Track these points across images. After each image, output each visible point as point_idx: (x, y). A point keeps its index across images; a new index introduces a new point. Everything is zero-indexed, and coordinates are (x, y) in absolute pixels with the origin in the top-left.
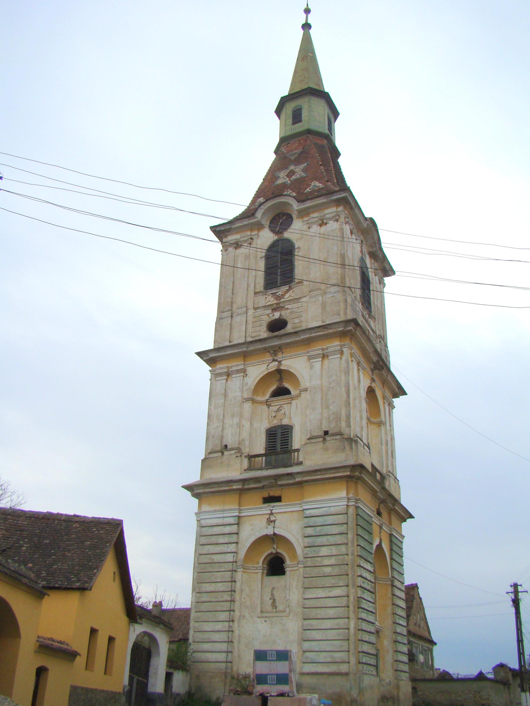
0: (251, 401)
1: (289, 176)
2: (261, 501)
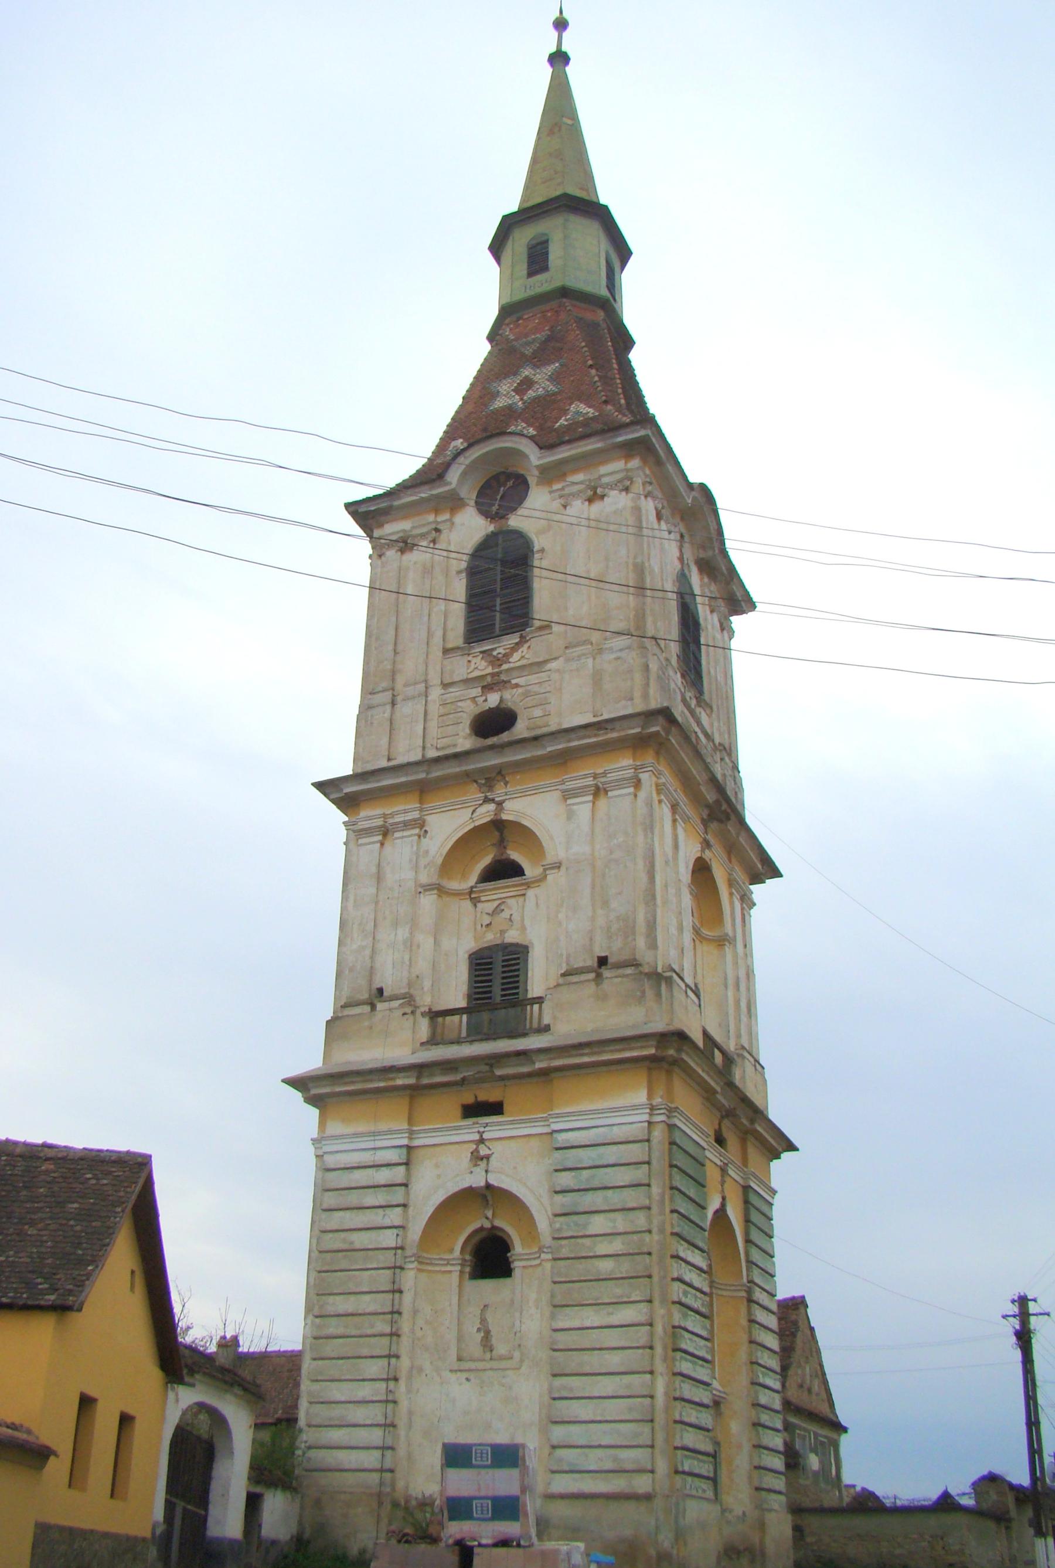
0: (435, 892)
1: (520, 390)
2: (458, 1112)
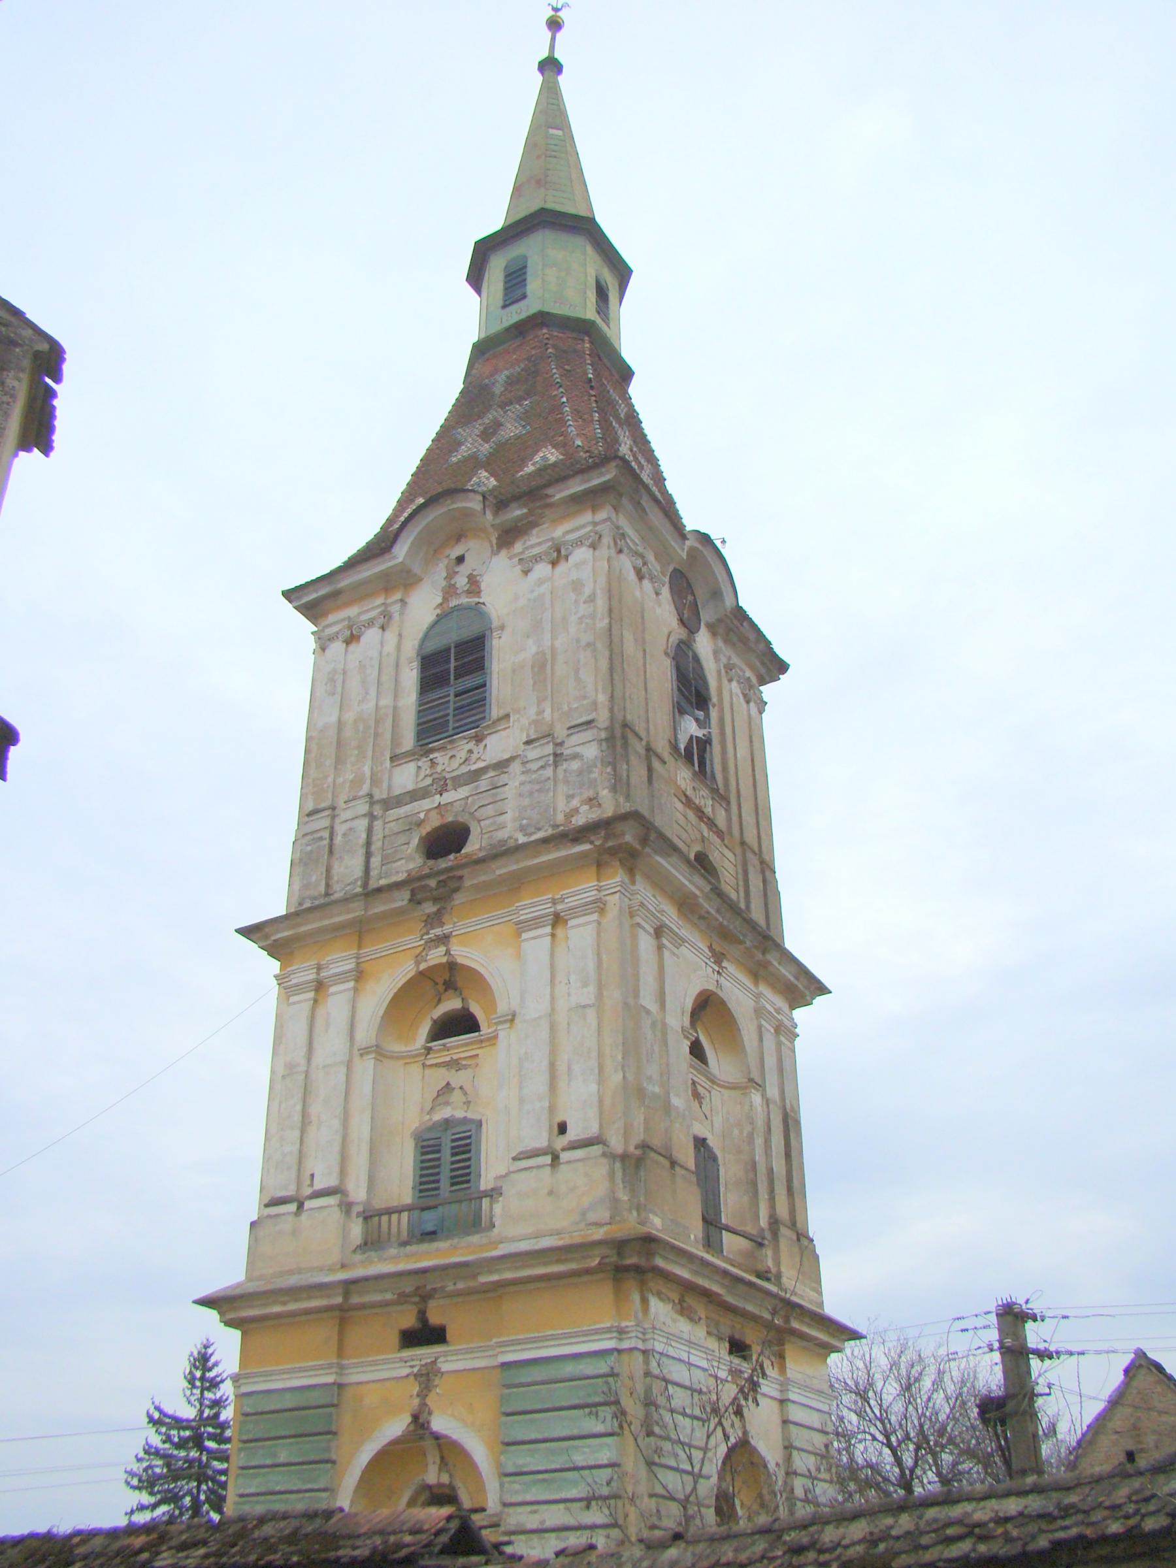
0: (373, 1055)
1: (486, 435)
2: (395, 1339)
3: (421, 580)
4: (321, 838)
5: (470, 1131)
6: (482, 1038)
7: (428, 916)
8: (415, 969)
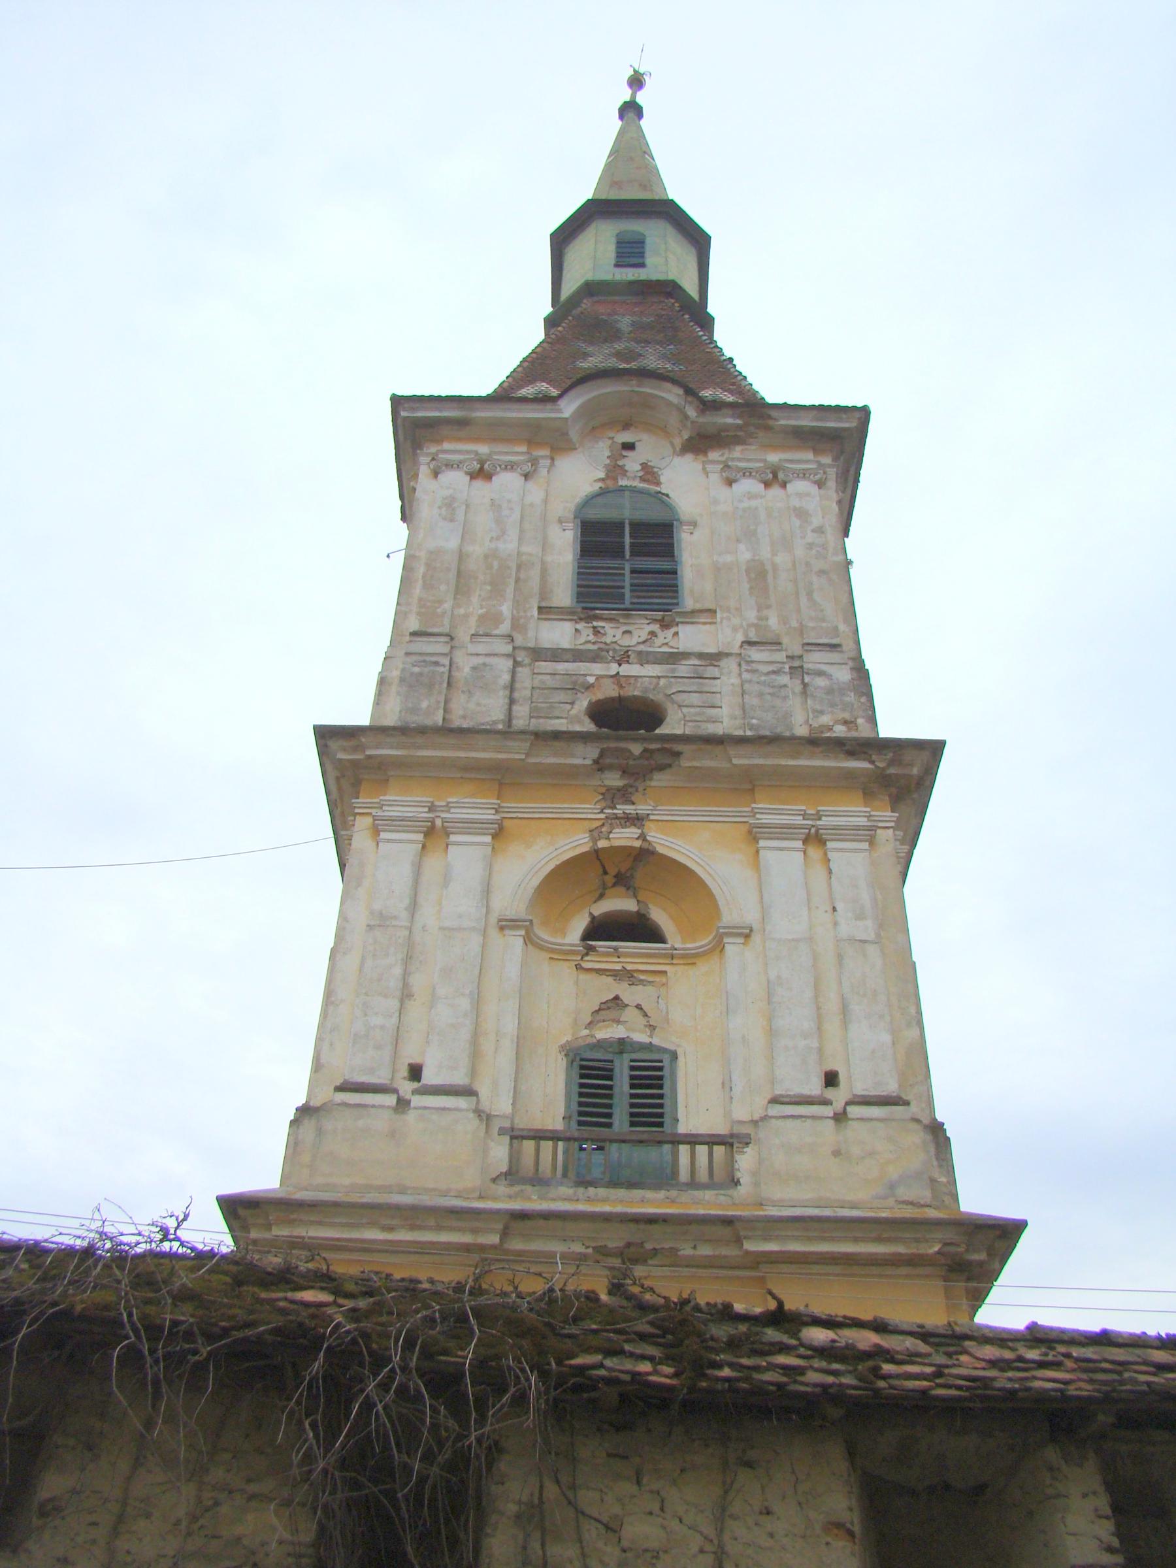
3: (576, 449)
4: (437, 664)
5: (661, 1061)
6: (675, 952)
7: (608, 790)
8: (591, 844)
